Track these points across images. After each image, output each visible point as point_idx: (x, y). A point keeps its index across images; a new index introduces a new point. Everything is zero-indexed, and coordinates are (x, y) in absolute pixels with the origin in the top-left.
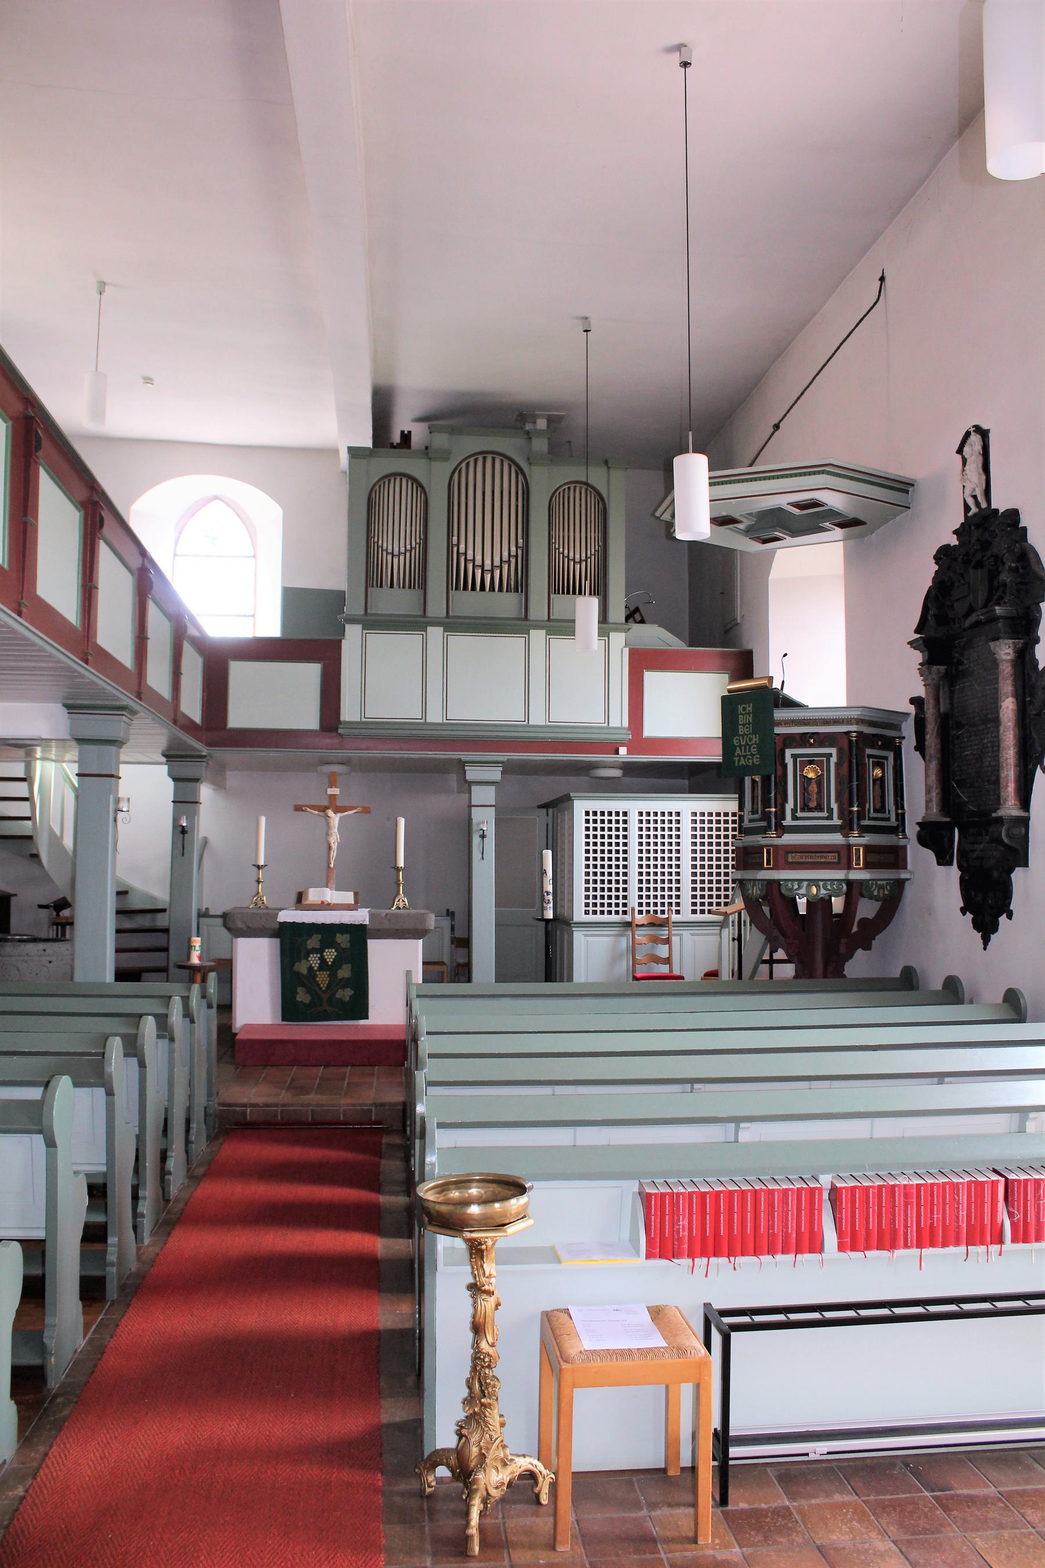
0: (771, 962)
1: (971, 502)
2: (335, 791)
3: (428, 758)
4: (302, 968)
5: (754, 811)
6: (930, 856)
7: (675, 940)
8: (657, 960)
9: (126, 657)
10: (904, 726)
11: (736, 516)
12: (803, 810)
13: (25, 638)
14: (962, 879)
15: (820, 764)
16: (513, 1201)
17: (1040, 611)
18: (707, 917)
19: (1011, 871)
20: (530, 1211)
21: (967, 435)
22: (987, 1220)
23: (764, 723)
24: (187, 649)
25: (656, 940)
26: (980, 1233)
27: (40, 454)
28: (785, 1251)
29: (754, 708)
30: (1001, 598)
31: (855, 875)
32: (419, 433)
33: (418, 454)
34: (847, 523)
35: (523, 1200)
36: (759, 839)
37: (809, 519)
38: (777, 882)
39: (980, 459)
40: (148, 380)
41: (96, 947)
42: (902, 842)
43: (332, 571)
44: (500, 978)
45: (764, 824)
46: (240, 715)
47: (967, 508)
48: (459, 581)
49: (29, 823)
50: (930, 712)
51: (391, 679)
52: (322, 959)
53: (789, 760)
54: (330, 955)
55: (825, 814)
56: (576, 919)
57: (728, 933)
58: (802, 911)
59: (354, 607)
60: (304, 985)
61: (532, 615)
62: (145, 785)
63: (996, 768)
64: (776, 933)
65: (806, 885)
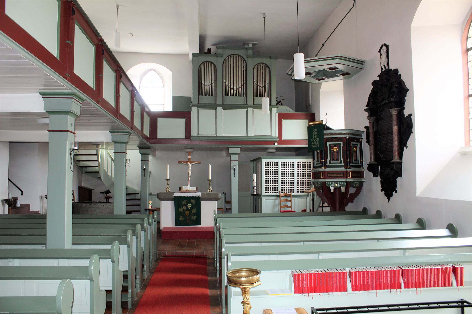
0: (323, 207)
1: (383, 67)
2: (190, 157)
3: (220, 145)
4: (181, 210)
5: (317, 161)
6: (371, 174)
7: (293, 200)
8: (287, 206)
9: (128, 117)
10: (363, 135)
11: (311, 72)
12: (332, 161)
13: (100, 111)
14: (381, 181)
15: (337, 147)
16: (255, 276)
17: (405, 100)
18: (302, 194)
19: (397, 178)
20: (260, 280)
21: (382, 46)
22: (396, 282)
23: (320, 134)
24: (145, 115)
25: (287, 200)
26: (395, 286)
27: (104, 56)
28: (336, 291)
29: (317, 130)
30: (393, 96)
31: (348, 180)
32: (213, 49)
33: (213, 55)
34: (345, 74)
35: (258, 276)
36: (320, 170)
37: (332, 73)
38: (325, 183)
39: (386, 54)
40: (131, 34)
41: (120, 205)
42: (362, 170)
43: (188, 91)
44: (240, 212)
45: (321, 165)
46: (161, 134)
47: (382, 69)
48: (226, 93)
49: (98, 168)
50: (371, 131)
51: (207, 123)
52: (187, 207)
53: (328, 146)
54: (189, 206)
55: (339, 162)
56: (263, 194)
57: (309, 198)
58: (332, 191)
59: (194, 101)
60: (181, 215)
61: (248, 103)
62: (133, 155)
63: (392, 147)
64: (325, 198)
65: (334, 183)
